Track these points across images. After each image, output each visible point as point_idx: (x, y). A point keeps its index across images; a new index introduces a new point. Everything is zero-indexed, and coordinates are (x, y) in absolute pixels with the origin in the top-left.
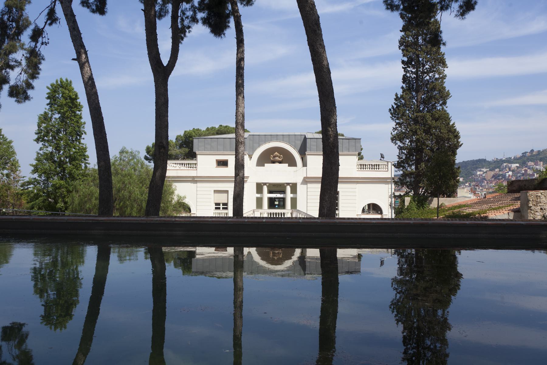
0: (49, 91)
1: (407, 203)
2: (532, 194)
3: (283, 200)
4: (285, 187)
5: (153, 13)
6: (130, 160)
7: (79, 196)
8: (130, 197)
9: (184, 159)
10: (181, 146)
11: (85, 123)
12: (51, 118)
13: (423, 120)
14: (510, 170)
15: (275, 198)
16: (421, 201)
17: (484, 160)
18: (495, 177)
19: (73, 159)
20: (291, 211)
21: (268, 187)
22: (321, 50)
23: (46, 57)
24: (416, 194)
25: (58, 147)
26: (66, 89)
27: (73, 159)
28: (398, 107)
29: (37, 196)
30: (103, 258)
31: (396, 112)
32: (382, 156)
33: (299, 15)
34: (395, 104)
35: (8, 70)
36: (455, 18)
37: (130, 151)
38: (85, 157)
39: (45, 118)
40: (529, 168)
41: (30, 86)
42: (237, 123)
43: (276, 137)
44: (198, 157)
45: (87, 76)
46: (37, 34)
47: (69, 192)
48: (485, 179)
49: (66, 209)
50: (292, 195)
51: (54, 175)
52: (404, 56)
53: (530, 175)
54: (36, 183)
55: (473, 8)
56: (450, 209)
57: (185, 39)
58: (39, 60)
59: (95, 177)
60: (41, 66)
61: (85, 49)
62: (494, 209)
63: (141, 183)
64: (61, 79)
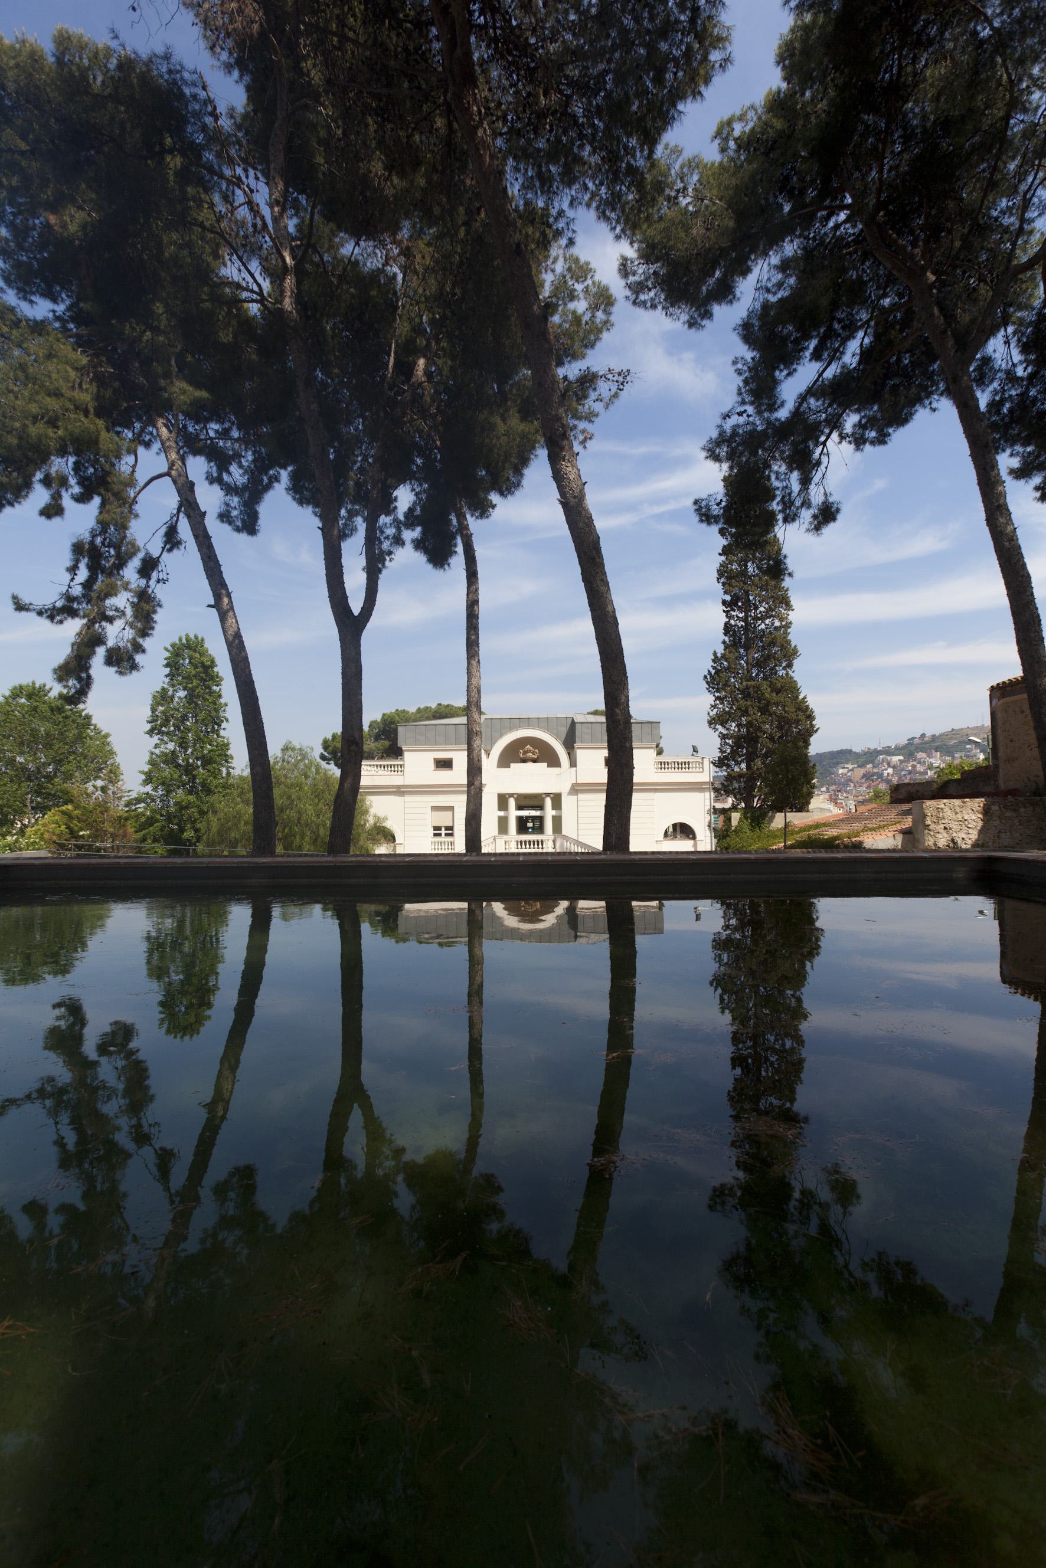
0: (168, 654)
1: (734, 822)
2: (930, 806)
3: (541, 819)
4: (543, 800)
5: (336, 532)
6: (298, 762)
7: (219, 819)
8: (299, 819)
9: (382, 758)
10: (377, 738)
11: (226, 705)
12: (173, 697)
13: (756, 692)
14: (889, 765)
15: (527, 818)
16: (757, 818)
17: (850, 752)
18: (867, 776)
19: (207, 761)
20: (552, 837)
21: (516, 800)
22: (603, 588)
23: (163, 602)
24: (749, 807)
25: (183, 742)
26: (195, 651)
27: (207, 761)
28: (717, 672)
29: (151, 821)
30: (260, 925)
31: (716, 680)
32: (695, 750)
33: (567, 532)
34: (714, 668)
35: (104, 624)
36: (806, 534)
37: (298, 747)
38: (227, 758)
39: (162, 698)
40: (919, 763)
41: (138, 648)
42: (468, 701)
43: (527, 722)
44: (406, 754)
45: (231, 632)
46: (149, 566)
47: (202, 813)
48: (851, 781)
49: (199, 839)
50: (554, 813)
51: (178, 788)
52: (725, 593)
53: (920, 773)
54: (149, 801)
55: (834, 519)
56: (802, 830)
57: (384, 572)
58: (154, 606)
59: (243, 788)
60: (156, 617)
61: (227, 590)
62: (871, 830)
63: (316, 797)
64: (187, 635)
